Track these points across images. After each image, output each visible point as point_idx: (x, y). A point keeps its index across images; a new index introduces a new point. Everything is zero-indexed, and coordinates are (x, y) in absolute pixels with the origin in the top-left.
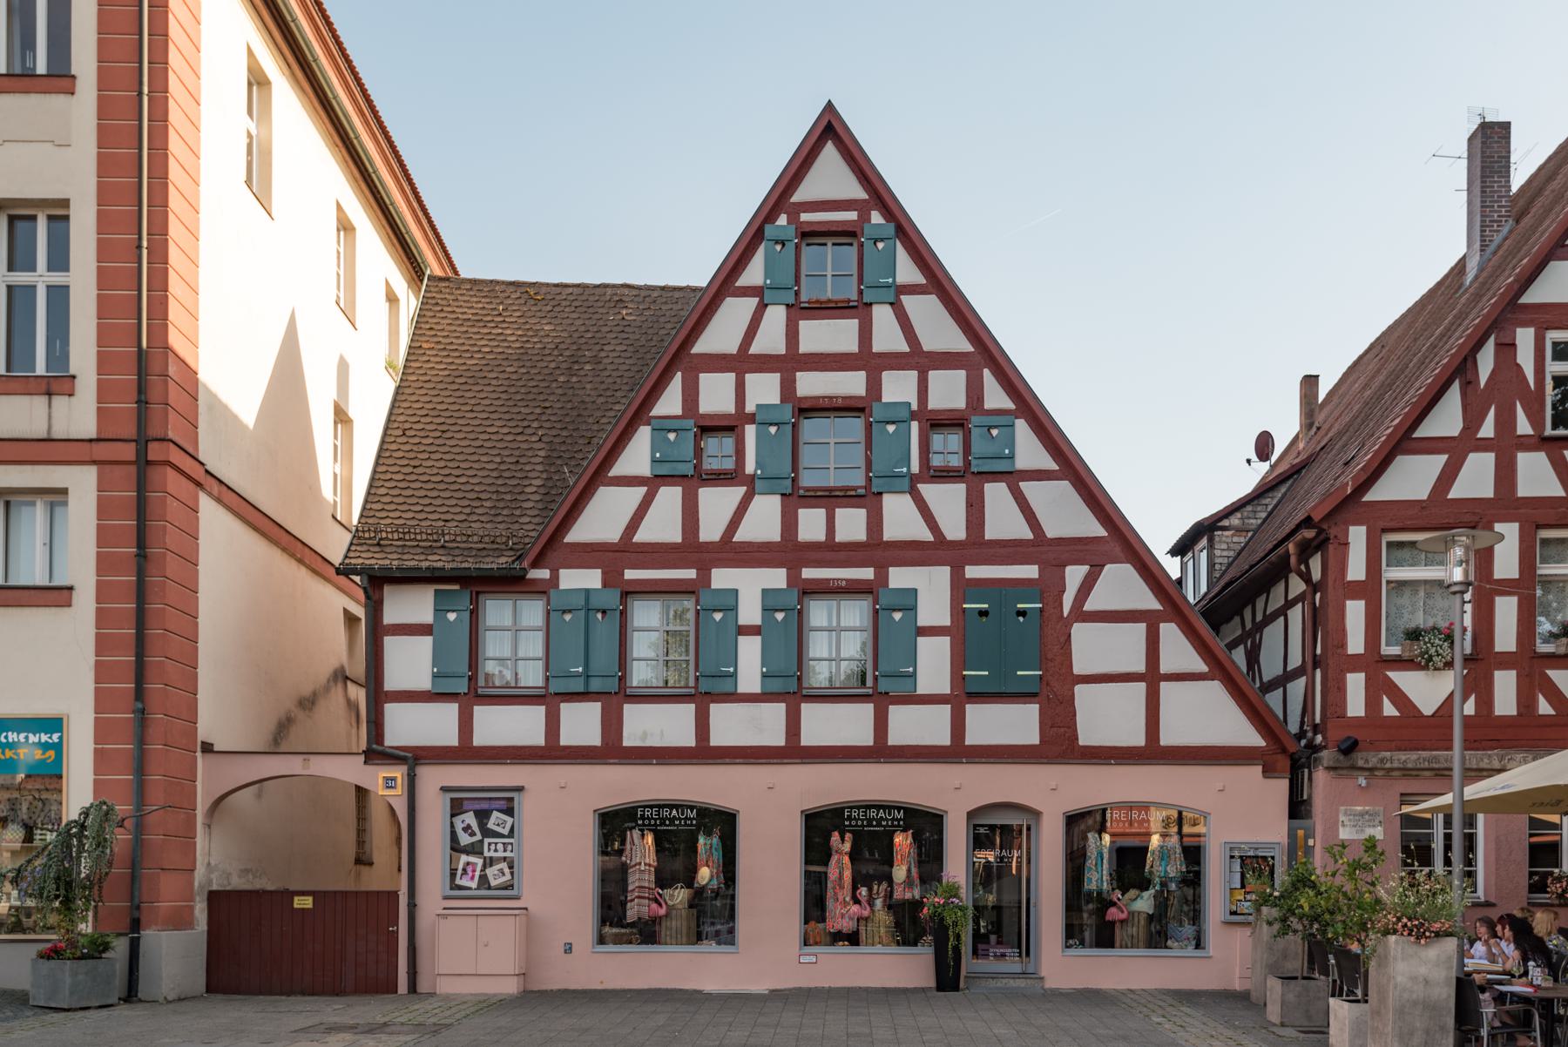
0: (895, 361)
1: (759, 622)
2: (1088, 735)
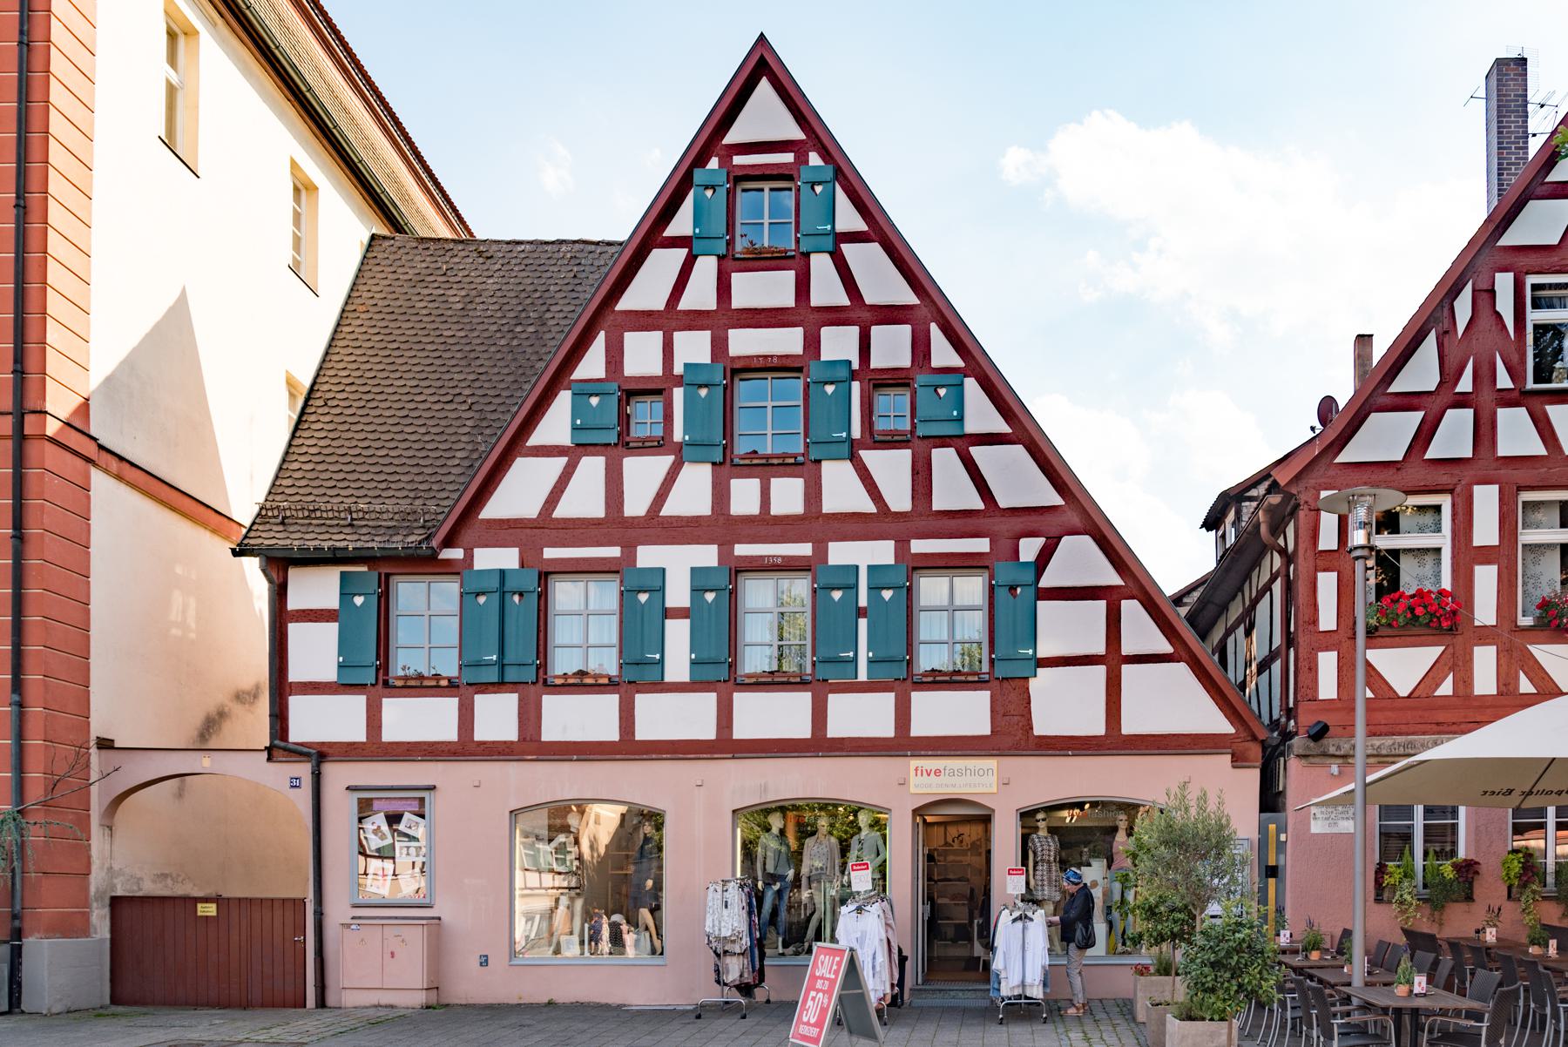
0: (835, 316)
1: (688, 604)
2: (1043, 725)
